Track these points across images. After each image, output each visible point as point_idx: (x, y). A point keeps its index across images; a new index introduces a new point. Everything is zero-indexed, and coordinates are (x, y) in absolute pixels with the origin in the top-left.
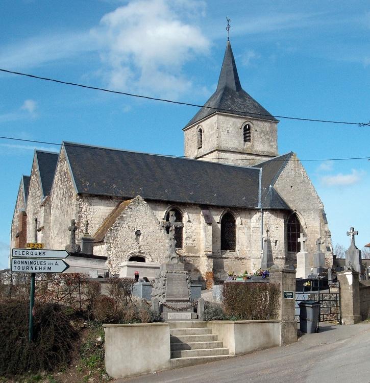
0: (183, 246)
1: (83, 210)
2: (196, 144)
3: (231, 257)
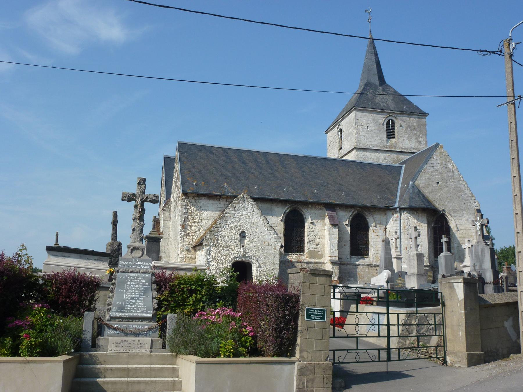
0: (305, 251)
1: (189, 211)
2: (337, 146)
3: (362, 263)
